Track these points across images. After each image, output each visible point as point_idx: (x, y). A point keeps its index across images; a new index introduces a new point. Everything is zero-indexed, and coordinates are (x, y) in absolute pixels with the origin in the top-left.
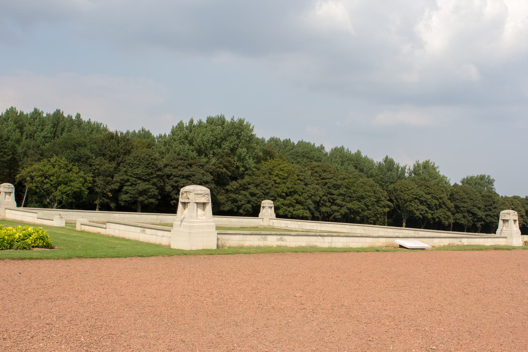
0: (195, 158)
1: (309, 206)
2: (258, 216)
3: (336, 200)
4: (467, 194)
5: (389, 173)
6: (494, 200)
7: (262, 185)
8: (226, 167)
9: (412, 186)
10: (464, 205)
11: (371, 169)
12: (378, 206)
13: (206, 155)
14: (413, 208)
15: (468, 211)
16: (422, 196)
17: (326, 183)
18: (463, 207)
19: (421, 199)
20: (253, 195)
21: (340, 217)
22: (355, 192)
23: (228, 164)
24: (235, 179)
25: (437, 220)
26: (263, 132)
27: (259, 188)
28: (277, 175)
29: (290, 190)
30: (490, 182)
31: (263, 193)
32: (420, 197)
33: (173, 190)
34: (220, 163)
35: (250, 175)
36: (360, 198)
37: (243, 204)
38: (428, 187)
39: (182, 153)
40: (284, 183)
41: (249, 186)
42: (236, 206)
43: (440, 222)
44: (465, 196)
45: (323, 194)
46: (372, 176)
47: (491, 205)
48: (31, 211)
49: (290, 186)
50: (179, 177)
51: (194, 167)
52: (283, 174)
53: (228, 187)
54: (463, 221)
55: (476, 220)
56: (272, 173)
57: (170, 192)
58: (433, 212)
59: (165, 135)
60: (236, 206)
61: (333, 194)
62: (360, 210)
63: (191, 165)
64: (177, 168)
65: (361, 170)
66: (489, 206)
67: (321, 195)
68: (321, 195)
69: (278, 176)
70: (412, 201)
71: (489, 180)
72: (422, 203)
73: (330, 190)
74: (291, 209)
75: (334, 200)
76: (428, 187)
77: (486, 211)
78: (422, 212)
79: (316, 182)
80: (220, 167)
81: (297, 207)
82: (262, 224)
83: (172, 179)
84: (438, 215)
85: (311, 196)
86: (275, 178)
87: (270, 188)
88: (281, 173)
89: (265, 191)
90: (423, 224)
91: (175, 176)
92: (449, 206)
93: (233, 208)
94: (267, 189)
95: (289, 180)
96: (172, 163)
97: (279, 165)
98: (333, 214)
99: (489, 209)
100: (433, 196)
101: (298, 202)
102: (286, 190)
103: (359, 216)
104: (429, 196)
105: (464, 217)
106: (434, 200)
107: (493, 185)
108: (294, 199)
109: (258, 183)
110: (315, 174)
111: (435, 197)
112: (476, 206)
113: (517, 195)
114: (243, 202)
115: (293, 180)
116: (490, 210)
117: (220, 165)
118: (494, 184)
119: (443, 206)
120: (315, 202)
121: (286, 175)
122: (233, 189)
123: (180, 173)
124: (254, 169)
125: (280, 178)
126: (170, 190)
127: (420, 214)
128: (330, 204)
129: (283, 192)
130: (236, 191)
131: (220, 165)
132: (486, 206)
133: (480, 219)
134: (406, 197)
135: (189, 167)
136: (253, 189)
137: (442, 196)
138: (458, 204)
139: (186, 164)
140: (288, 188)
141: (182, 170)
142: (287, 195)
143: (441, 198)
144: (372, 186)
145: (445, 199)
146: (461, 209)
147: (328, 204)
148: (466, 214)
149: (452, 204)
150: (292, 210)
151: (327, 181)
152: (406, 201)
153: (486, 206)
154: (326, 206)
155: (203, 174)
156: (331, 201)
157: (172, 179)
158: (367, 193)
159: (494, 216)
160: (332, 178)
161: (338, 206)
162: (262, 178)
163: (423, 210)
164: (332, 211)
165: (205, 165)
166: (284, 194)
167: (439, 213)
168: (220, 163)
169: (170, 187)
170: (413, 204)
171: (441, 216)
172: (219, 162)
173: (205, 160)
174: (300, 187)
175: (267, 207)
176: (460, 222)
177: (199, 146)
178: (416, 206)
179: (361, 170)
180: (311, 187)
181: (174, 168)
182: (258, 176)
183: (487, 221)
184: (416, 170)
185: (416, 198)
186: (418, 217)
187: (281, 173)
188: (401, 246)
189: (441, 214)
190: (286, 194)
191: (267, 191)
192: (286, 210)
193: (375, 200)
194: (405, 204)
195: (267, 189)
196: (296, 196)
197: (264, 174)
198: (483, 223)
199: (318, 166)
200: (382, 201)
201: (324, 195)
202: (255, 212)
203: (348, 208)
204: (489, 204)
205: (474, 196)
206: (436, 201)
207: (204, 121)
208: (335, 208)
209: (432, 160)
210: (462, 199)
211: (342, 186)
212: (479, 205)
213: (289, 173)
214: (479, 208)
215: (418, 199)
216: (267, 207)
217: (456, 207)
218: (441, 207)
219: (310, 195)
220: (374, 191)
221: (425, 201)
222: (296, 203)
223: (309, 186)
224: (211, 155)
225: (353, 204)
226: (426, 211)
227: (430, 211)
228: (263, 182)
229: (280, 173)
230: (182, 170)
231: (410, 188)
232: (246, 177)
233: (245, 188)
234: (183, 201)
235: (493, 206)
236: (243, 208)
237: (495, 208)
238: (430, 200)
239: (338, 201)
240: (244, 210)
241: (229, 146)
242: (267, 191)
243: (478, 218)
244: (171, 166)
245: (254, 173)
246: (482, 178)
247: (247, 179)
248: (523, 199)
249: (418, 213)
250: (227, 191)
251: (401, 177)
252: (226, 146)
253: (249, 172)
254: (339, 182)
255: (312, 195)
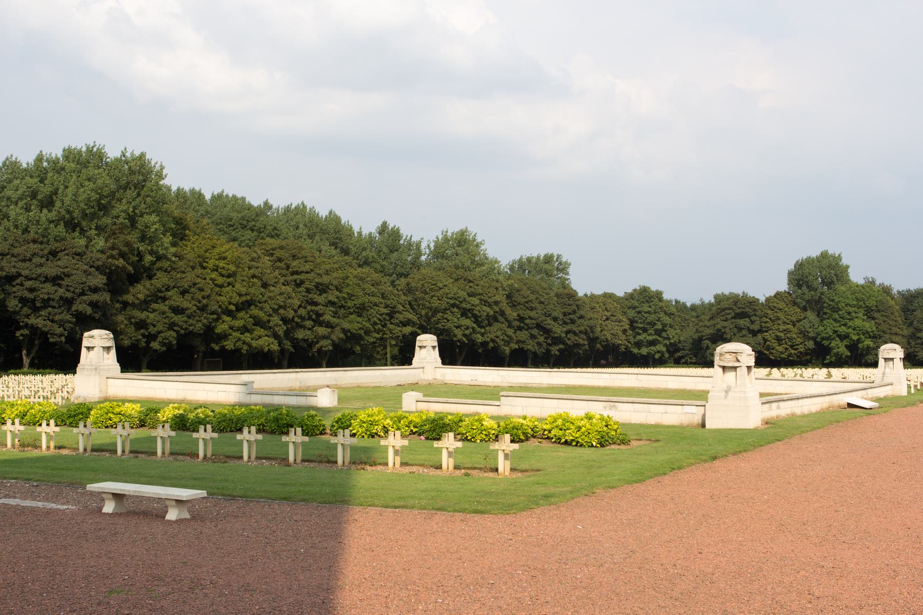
0: (63, 239)
1: (276, 329)
2: (410, 364)
3: (322, 315)
4: (532, 293)
5: (395, 255)
6: (579, 303)
7: (193, 290)
8: (122, 255)
9: (444, 280)
10: (532, 314)
11: (364, 249)
12: (392, 323)
13: (83, 232)
14: (449, 325)
15: (539, 326)
16: (465, 300)
17: (302, 282)
18: (531, 318)
19: (464, 305)
20: (177, 310)
21: (331, 348)
22: (350, 296)
23: (126, 249)
24: (134, 279)
25: (491, 345)
26: (177, 179)
27: (188, 296)
28: (216, 269)
29: (244, 298)
30: (563, 268)
31: (199, 308)
32: (461, 302)
33: (22, 308)
34: (113, 248)
35: (166, 271)
36: (361, 310)
37: (161, 332)
38: (470, 281)
39: (33, 229)
40: (229, 284)
41: (169, 293)
42: (144, 336)
43: (496, 349)
44: (532, 297)
45: (299, 303)
46: (366, 263)
47: (574, 312)
48: (162, 378)
49: (243, 290)
50: (35, 279)
51: (65, 260)
52: (226, 266)
53: (129, 298)
54: (531, 346)
55: (549, 341)
56: (205, 264)
57: (17, 313)
58: (483, 330)
59: (538, 257)
60: (144, 336)
61: (316, 304)
62: (362, 332)
63: (54, 254)
64: (30, 260)
65: (345, 252)
66: (570, 314)
67: (296, 307)
68: (296, 307)
69: (217, 270)
70: (446, 309)
71: (560, 264)
72: (464, 313)
73: (310, 296)
74: (247, 337)
75: (319, 315)
76: (470, 281)
77: (565, 323)
78: (467, 332)
79: (282, 280)
80: (112, 257)
81: (256, 333)
82: (423, 376)
83: (22, 285)
84: (492, 336)
85: (278, 310)
86: (214, 275)
87: (208, 297)
88: (222, 264)
89: (200, 302)
90: (460, 354)
91: (28, 278)
92: (511, 318)
93: (138, 340)
94: (204, 298)
95: (238, 278)
96: (15, 251)
97: (214, 247)
98: (317, 343)
99: (571, 319)
100: (481, 300)
101: (258, 323)
102: (236, 299)
103: (360, 345)
104: (475, 301)
105: (533, 337)
106: (485, 308)
107: (567, 274)
108: (250, 317)
109: (186, 286)
110: (278, 264)
111: (486, 302)
112: (550, 315)
113: (610, 291)
114: (160, 327)
115: (245, 278)
116: (573, 322)
117: (115, 252)
118: (571, 270)
119: (500, 318)
120: (285, 320)
121: (232, 268)
122: (137, 302)
123: (39, 271)
124: (173, 259)
125: (223, 276)
126: (17, 309)
127: (464, 335)
128: (312, 323)
129: (230, 303)
130: (144, 305)
131: (115, 252)
132: (565, 314)
133: (557, 340)
134: (435, 303)
135: (51, 257)
136: (176, 299)
137: (497, 298)
138: (521, 312)
139: (46, 252)
140: (240, 295)
141: (41, 265)
142: (238, 309)
143: (496, 303)
144: (376, 284)
145: (504, 305)
146: (527, 321)
147: (308, 323)
148: (535, 332)
149: (515, 314)
150: (248, 340)
151: (302, 277)
152: (436, 311)
153: (565, 314)
154: (304, 327)
155: (85, 272)
156: (314, 317)
157: (22, 285)
158: (371, 299)
159: (581, 332)
160: (312, 270)
161: (327, 326)
162: (190, 276)
163: (467, 328)
164: (315, 337)
165: (85, 253)
166: (233, 308)
167: (495, 332)
168: (113, 248)
169: (16, 302)
170: (448, 315)
171: (497, 337)
172: (109, 244)
173: (83, 242)
174: (256, 291)
175: (427, 347)
176: (526, 347)
177: (68, 212)
178: (456, 320)
179: (345, 252)
180: (276, 290)
181: (24, 261)
182: (183, 272)
183: (569, 342)
184: (440, 251)
185: (453, 306)
186: (459, 341)
187: (222, 264)
188: (850, 405)
189: (499, 333)
190: (236, 305)
191: (205, 301)
192: (239, 339)
193: (386, 311)
194: (433, 316)
195: (204, 298)
196: (254, 311)
197: (193, 268)
198: (562, 346)
199: (282, 248)
200: (398, 312)
201: (300, 306)
202: (405, 357)
203: (344, 331)
204: (570, 311)
205: (546, 297)
206: (488, 309)
207: (231, 195)
208: (322, 331)
209: (472, 230)
210: (527, 302)
211: (331, 287)
212: (555, 314)
213: (237, 263)
214: (555, 319)
215: (458, 307)
216: (427, 347)
217: (521, 319)
218: (497, 320)
219: (276, 307)
220: (383, 294)
221: (469, 310)
222: (254, 325)
223: (272, 288)
224: (93, 232)
225: (349, 322)
226: (473, 328)
227: (478, 329)
228: (195, 284)
229: (221, 265)
230: (41, 265)
231: (441, 285)
232: (159, 274)
233: (161, 297)
234: (723, 364)
235: (578, 315)
236: (160, 339)
237: (581, 317)
238: (478, 308)
239: (327, 317)
240: (162, 344)
241: (125, 211)
242: (205, 301)
243: (554, 338)
244: (13, 255)
245: (174, 266)
246: (548, 259)
247: (161, 279)
248: (620, 298)
249: (459, 333)
250: (125, 304)
251: (416, 264)
252: (120, 208)
253: (165, 264)
254: (326, 279)
255: (280, 307)
